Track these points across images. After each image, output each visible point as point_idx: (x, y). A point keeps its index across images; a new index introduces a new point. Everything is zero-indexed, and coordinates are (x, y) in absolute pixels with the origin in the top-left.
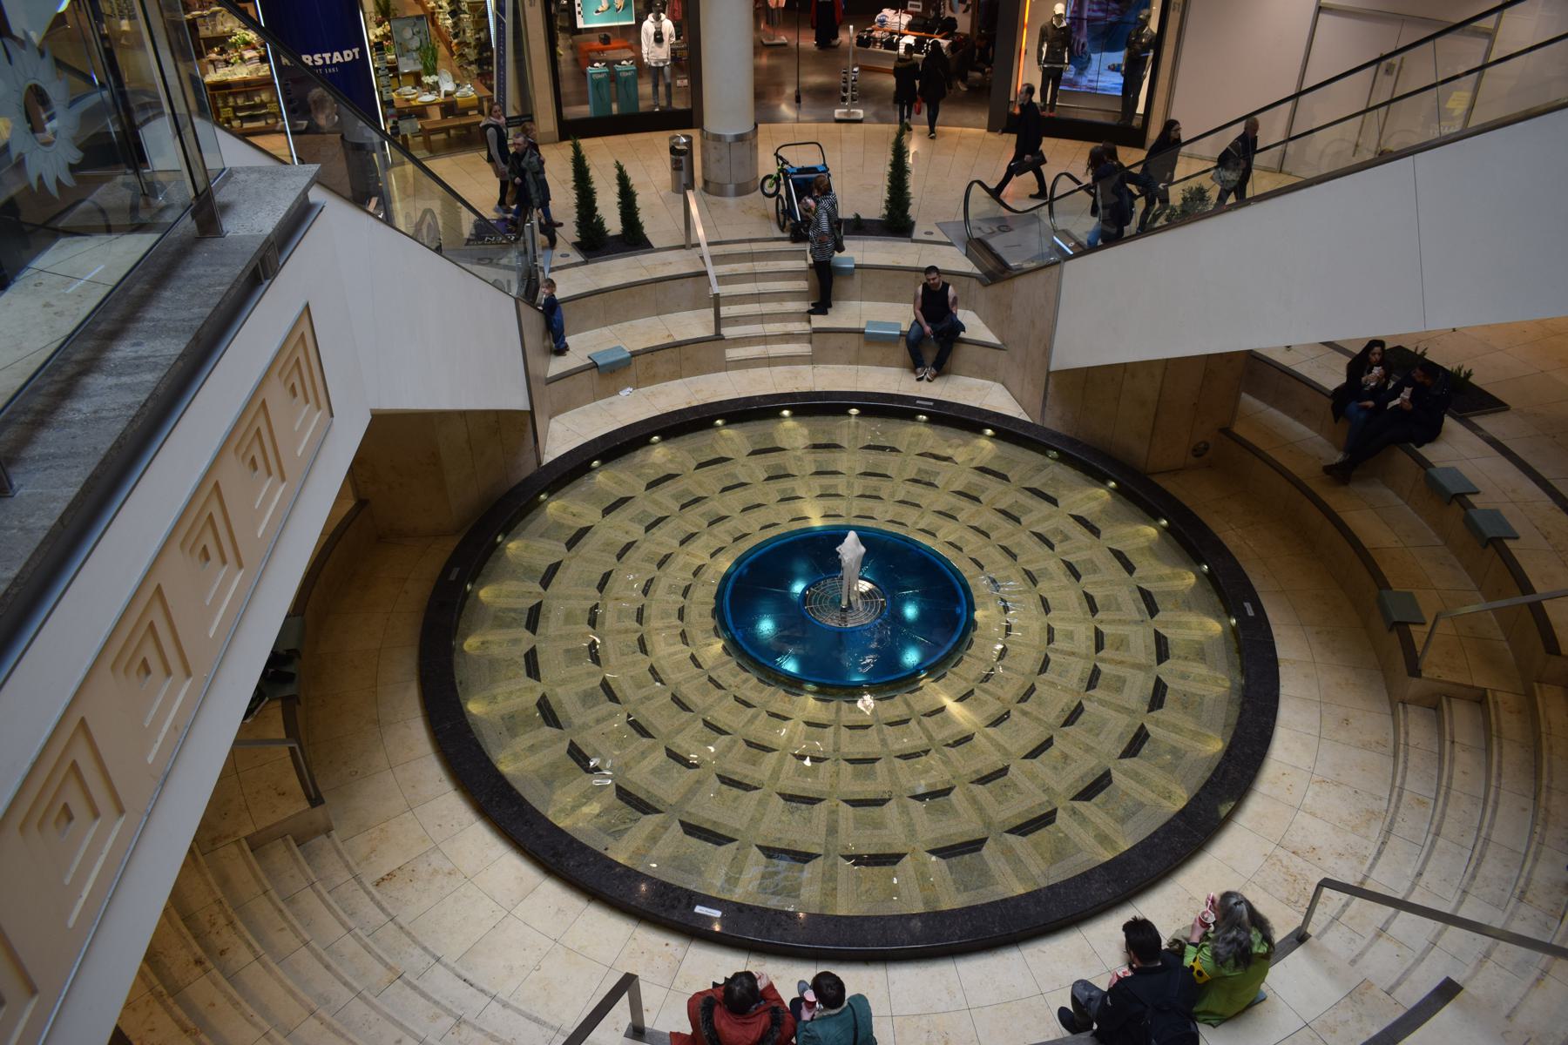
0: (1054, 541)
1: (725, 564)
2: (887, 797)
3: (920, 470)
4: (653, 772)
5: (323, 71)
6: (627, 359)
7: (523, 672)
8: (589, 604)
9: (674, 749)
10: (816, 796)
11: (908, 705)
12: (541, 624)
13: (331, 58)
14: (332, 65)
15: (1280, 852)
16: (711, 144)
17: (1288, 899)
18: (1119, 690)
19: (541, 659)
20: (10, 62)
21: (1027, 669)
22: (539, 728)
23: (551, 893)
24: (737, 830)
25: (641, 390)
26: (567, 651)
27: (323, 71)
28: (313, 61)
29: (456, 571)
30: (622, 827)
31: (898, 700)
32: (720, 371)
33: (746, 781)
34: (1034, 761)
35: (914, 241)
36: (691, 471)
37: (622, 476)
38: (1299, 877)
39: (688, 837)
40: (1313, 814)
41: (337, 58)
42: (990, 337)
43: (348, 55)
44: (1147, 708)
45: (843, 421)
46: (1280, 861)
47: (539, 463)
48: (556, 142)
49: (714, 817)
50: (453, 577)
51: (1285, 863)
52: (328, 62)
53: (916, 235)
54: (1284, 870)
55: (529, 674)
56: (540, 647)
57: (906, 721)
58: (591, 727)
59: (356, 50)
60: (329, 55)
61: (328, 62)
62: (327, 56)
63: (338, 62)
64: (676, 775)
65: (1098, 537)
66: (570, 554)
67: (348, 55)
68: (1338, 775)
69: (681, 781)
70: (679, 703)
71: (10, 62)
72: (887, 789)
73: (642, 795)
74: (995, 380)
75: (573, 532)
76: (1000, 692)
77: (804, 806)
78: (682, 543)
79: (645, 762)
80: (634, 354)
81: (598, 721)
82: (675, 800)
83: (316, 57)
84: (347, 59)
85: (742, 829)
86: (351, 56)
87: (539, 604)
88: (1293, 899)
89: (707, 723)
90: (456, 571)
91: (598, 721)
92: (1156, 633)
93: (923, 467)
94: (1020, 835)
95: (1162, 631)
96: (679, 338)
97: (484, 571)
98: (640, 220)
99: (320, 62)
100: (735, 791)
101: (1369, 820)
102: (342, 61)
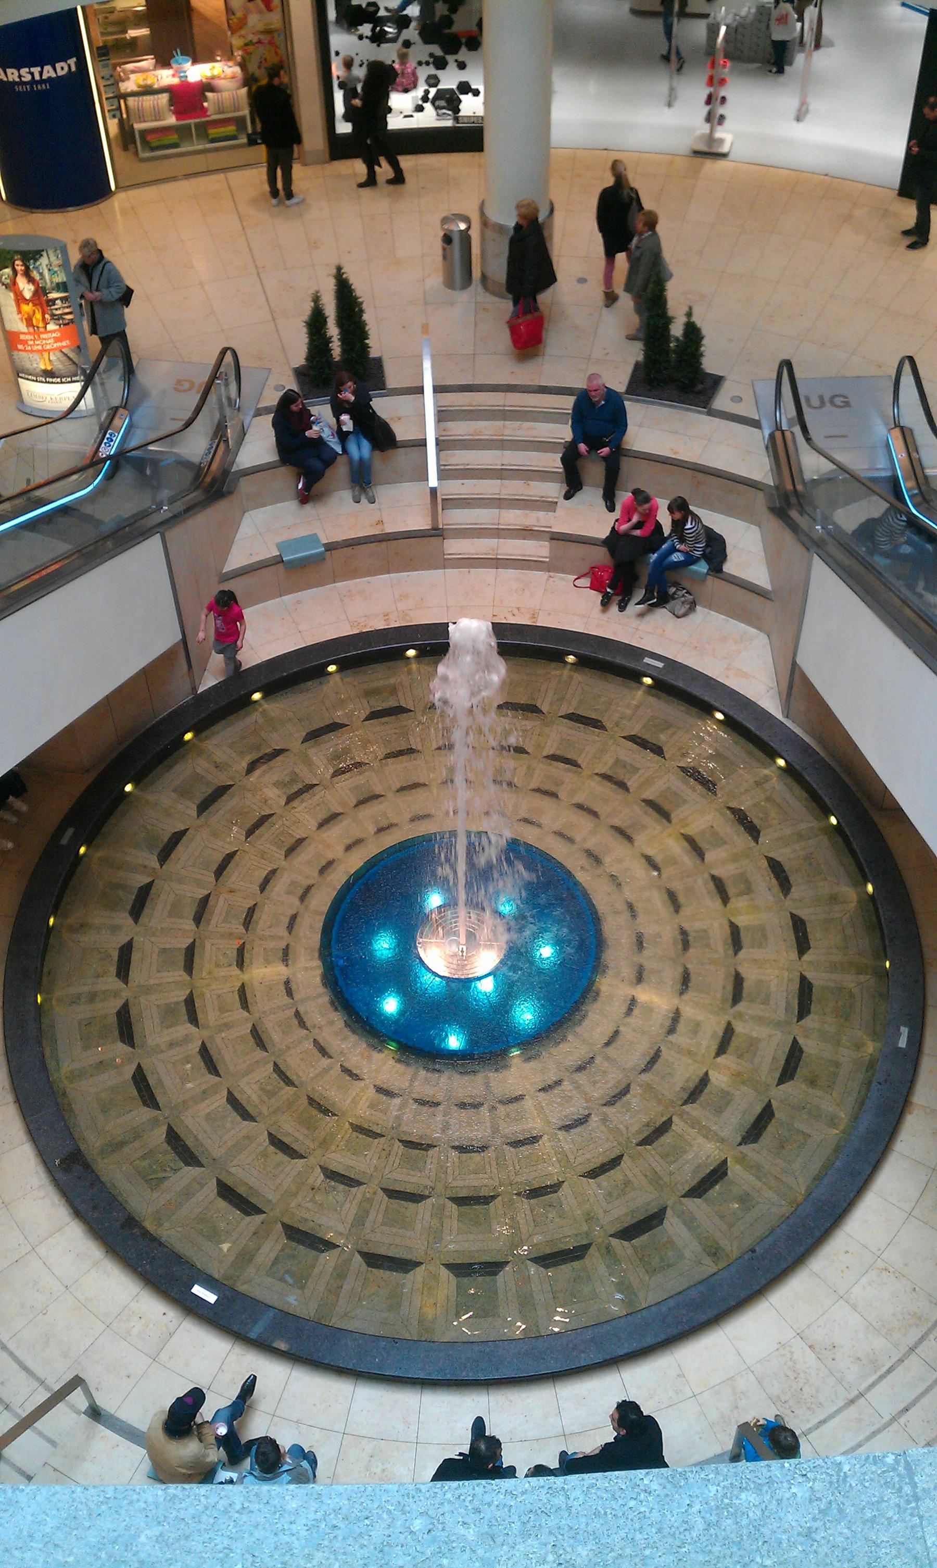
0: (731, 891)
1: (355, 862)
2: (427, 1193)
3: (617, 761)
4: (208, 1117)
5: (32, 88)
6: (321, 554)
7: (113, 970)
8: (201, 893)
9: (236, 1094)
10: (357, 1177)
11: (487, 1085)
12: (146, 911)
13: (41, 73)
14: (42, 81)
15: (798, 1345)
16: (489, 233)
17: (778, 1397)
18: (719, 1111)
19: (135, 956)
20: (826, 437)
21: (630, 1065)
22: (113, 1042)
23: (927, 426)
24: (269, 1201)
25: (338, 585)
26: (164, 950)
27: (32, 88)
28: (20, 76)
29: (70, 832)
30: (164, 1175)
31: (479, 1079)
32: (436, 568)
33: (295, 1146)
34: (591, 1181)
35: (712, 413)
36: (359, 722)
37: (73, 991)
38: (802, 1375)
39: (220, 1200)
40: (854, 1307)
41: (48, 72)
42: (759, 575)
43: (62, 69)
44: (739, 1139)
45: (556, 672)
46: (792, 1353)
47: (194, 689)
48: (326, 163)
49: (252, 1181)
50: (64, 841)
51: (795, 1357)
52: (37, 77)
53: (721, 402)
54: (790, 1364)
55: (118, 975)
56: (139, 940)
57: (476, 1106)
58: (162, 1051)
59: (72, 61)
60: (39, 69)
61: (37, 77)
62: (36, 70)
63: (50, 78)
64: (228, 1125)
65: (786, 895)
66: (198, 822)
67: (62, 69)
68: (906, 1265)
69: (233, 1132)
70: (258, 1038)
71: (826, 437)
72: (429, 1183)
73: (190, 1142)
74: (759, 628)
75: (210, 791)
76: (588, 1088)
77: (341, 1187)
78: (321, 825)
79: (204, 1105)
80: (331, 547)
81: (171, 1045)
82: (219, 1154)
83: (24, 71)
84: (61, 73)
85: (274, 1201)
86: (66, 69)
87: (150, 885)
88: (783, 1398)
89: (277, 1069)
90: (70, 832)
91: (171, 1045)
92: (795, 1041)
93: (622, 758)
94: (541, 1266)
95: (801, 1041)
96: (390, 528)
97: (104, 830)
98: (374, 353)
99: (28, 78)
100: (281, 1157)
101: (910, 1326)
102: (54, 75)
